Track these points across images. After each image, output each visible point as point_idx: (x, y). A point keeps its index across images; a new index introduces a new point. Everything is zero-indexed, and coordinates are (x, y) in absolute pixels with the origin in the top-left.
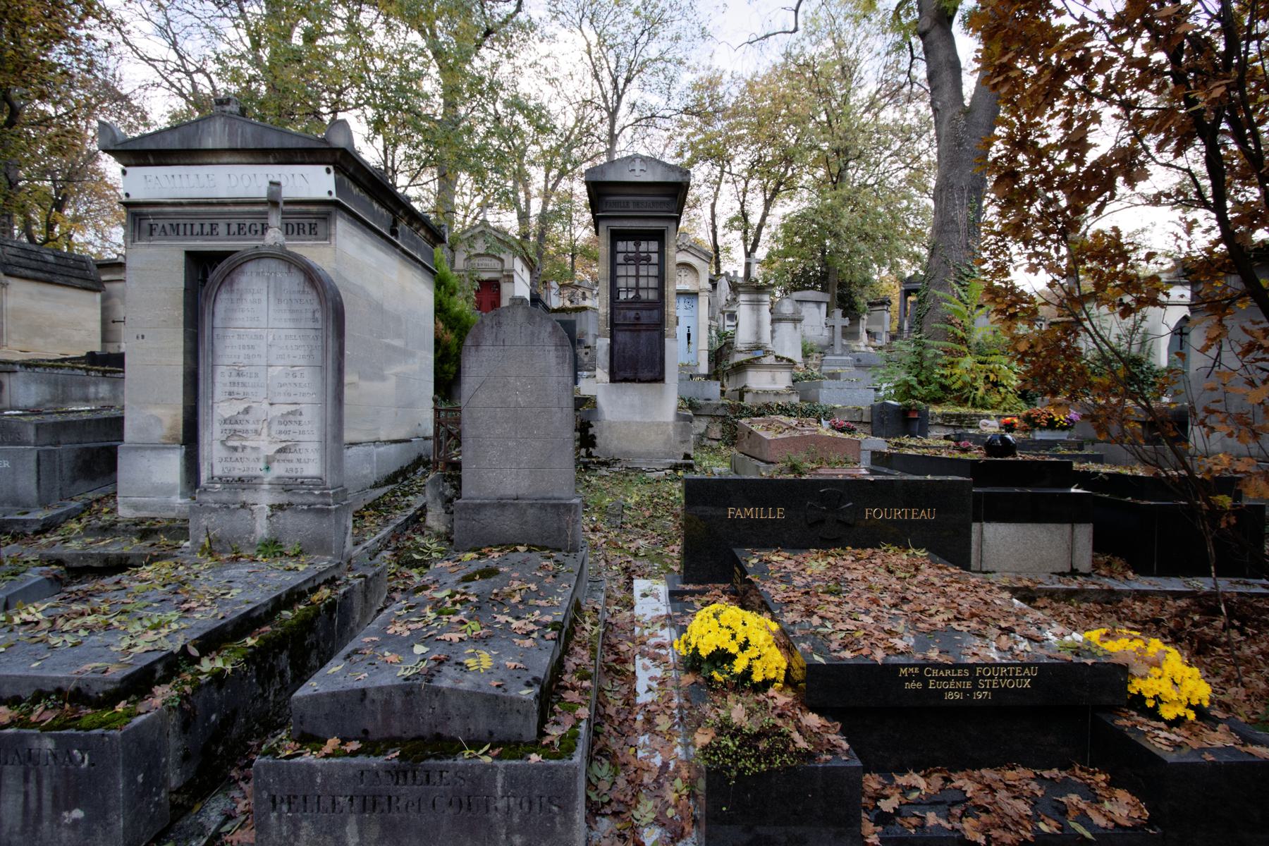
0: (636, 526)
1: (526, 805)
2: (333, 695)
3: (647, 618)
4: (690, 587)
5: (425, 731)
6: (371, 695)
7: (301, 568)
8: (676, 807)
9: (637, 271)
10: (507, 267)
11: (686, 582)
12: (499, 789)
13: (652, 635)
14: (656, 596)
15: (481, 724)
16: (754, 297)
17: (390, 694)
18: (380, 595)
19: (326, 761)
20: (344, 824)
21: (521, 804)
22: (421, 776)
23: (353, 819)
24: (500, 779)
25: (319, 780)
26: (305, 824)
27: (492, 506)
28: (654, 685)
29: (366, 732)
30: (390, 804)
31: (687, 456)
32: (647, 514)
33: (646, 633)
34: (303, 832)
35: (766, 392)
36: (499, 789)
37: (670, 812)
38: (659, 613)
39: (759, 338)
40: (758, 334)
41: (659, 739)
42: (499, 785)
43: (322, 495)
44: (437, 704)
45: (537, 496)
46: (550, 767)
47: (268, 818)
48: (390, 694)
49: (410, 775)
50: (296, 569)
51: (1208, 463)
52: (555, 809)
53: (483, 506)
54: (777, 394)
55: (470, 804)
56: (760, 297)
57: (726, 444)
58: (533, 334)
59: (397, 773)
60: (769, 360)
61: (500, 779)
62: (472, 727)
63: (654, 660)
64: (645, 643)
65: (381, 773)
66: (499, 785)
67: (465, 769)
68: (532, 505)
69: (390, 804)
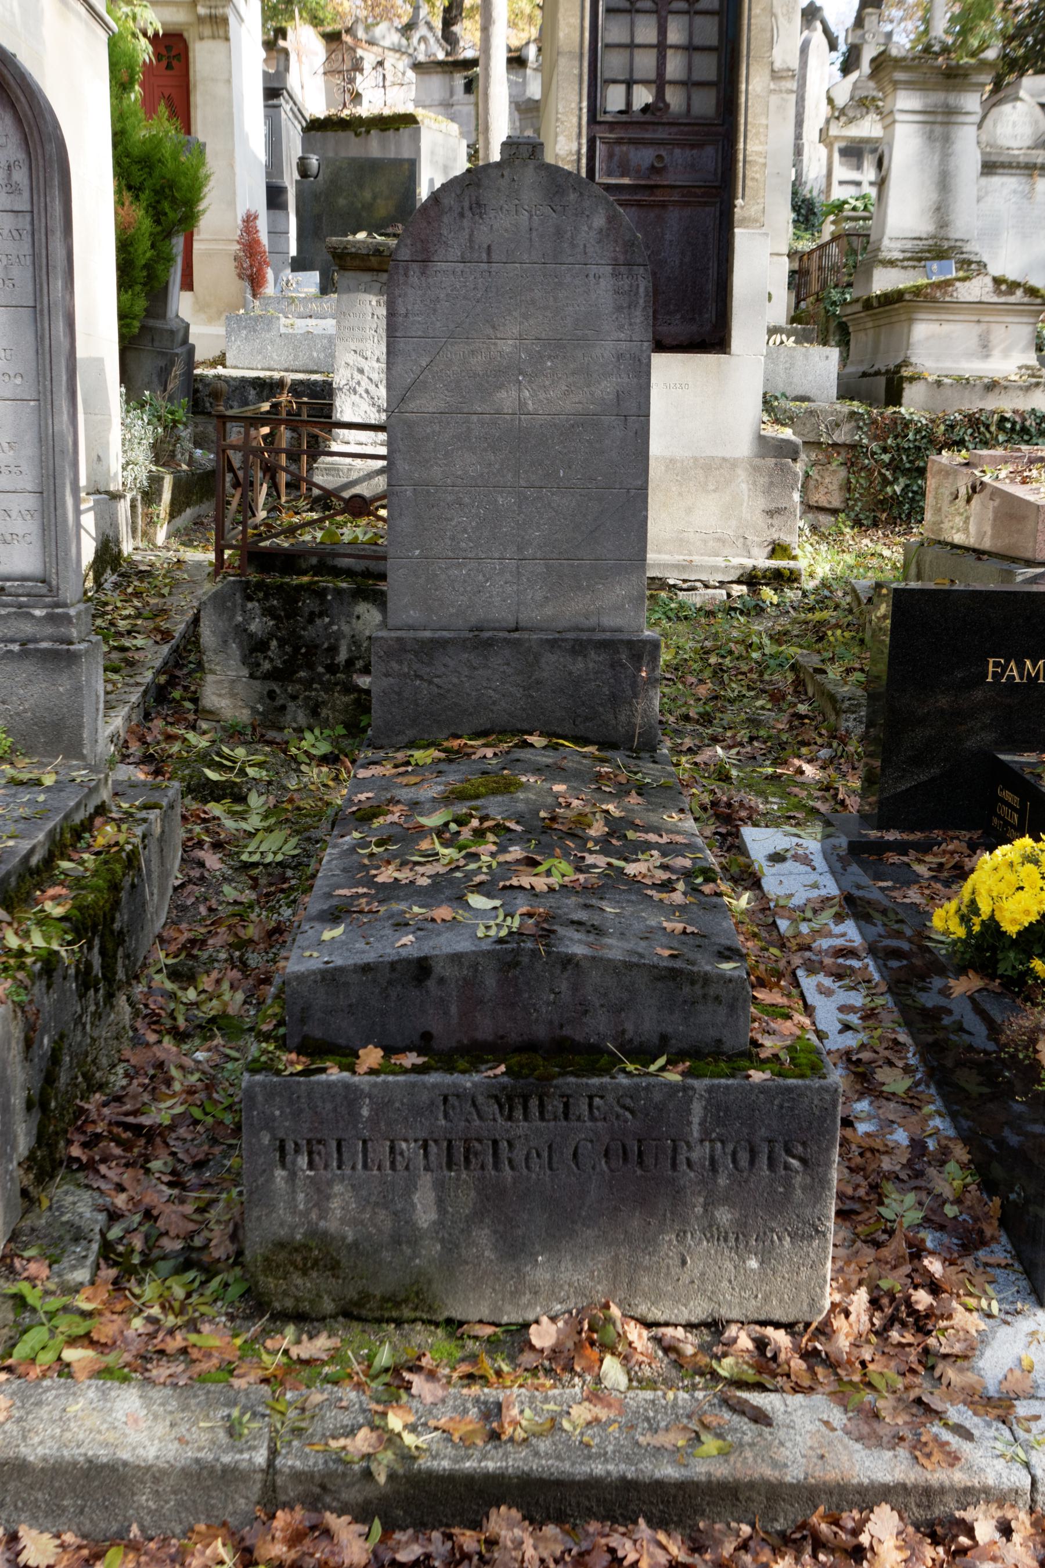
0: (686, 718)
1: (744, 1157)
2: (366, 969)
3: (798, 900)
4: (891, 836)
5: (541, 1032)
6: (438, 969)
7: (49, 780)
8: (958, 1201)
9: (662, 31)
11: (883, 825)
12: (696, 1128)
13: (817, 933)
14: (805, 860)
15: (646, 1021)
16: (937, 98)
17: (475, 967)
18: (175, 851)
19: (373, 1078)
20: (411, 1187)
21: (734, 1154)
22: (555, 1105)
23: (426, 1180)
24: (697, 1109)
25: (365, 1112)
26: (338, 1188)
27: (462, 644)
28: (854, 1019)
29: (427, 1036)
30: (496, 1154)
31: (778, 550)
32: (703, 691)
33: (804, 928)
34: (335, 1204)
35: (964, 383)
36: (696, 1128)
37: (951, 1211)
38: (823, 892)
40: (941, 212)
41: (892, 1105)
42: (696, 1120)
43: (51, 618)
44: (564, 986)
46: (789, 1089)
47: (271, 1179)
48: (475, 967)
49: (534, 1103)
50: (38, 783)
51: (874, 18)
52: (795, 1163)
53: (441, 644)
54: (992, 386)
55: (640, 1153)
56: (952, 99)
57: (857, 523)
58: (559, 233)
59: (510, 1098)
60: (977, 289)
61: (697, 1109)
62: (630, 1027)
63: (839, 977)
64: (809, 948)
65: (480, 1100)
66: (696, 1120)
67: (633, 1093)
68: (553, 644)
69: (496, 1154)
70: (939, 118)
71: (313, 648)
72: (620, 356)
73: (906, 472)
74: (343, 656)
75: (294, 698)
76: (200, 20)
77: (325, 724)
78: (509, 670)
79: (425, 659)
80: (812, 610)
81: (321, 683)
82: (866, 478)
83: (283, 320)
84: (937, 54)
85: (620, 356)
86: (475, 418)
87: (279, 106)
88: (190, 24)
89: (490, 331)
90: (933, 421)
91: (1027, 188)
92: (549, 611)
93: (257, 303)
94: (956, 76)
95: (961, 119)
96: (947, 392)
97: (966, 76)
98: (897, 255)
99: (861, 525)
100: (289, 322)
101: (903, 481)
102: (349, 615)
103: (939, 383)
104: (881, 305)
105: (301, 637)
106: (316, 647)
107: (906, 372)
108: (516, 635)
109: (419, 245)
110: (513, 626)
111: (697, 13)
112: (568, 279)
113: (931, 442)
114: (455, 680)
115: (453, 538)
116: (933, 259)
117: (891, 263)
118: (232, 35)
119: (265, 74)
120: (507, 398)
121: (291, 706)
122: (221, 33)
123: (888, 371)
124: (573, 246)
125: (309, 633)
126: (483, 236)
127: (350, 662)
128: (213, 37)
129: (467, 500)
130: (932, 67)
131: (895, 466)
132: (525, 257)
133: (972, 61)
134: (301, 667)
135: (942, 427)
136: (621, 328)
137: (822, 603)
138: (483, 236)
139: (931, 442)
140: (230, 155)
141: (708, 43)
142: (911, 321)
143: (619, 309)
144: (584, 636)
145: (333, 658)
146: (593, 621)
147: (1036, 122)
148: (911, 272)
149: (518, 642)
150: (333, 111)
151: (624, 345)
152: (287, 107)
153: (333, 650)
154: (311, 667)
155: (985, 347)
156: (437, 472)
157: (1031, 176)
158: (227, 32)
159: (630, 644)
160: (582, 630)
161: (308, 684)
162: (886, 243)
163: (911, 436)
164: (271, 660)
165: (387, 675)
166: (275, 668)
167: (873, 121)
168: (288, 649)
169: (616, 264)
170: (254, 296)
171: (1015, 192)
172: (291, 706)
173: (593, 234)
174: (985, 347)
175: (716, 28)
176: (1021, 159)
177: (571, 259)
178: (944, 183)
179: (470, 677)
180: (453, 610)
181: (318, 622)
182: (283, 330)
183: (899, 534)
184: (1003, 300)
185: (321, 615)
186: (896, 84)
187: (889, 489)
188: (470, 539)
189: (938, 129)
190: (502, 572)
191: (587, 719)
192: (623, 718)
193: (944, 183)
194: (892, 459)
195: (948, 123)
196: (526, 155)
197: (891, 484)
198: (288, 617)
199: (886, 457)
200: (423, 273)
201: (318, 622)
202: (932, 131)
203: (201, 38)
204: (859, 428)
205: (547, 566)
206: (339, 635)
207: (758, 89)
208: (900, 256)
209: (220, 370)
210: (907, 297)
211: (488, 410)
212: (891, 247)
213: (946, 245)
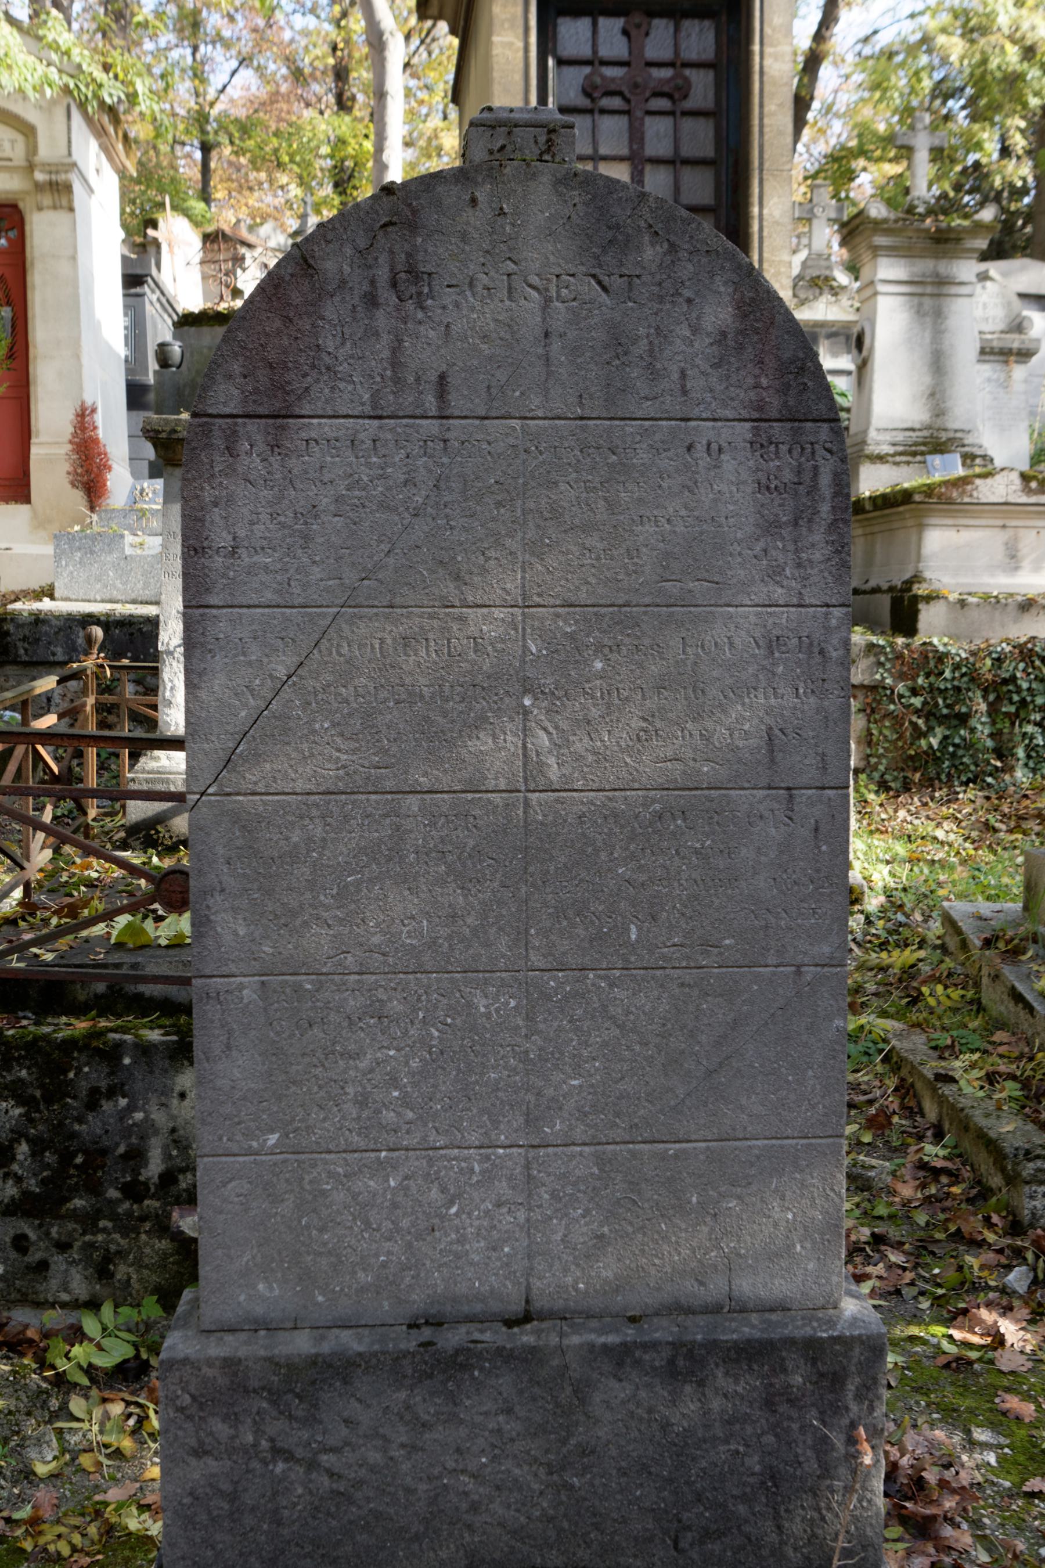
9: (636, 135)
10: (45, 152)
16: (925, 266)
27: (389, 1366)
35: (993, 602)
39: (939, 411)
40: (937, 397)
45: (638, 1299)
53: (334, 1371)
56: (944, 267)
57: (883, 786)
58: (618, 343)
68: (621, 1357)
70: (929, 290)
71: (97, 1154)
72: (773, 644)
73: (942, 720)
74: (154, 1168)
75: (63, 1247)
76: (38, 187)
77: (123, 1297)
78: (511, 1427)
79: (299, 1410)
80: (883, 946)
81: (114, 1217)
82: (892, 727)
83: (129, 538)
84: (923, 217)
85: (773, 644)
86: (413, 802)
87: (142, 295)
88: (27, 193)
89: (450, 589)
90: (973, 654)
91: (1003, 376)
92: (606, 1269)
93: (95, 517)
94: (947, 241)
95: (954, 290)
96: (974, 614)
97: (958, 240)
98: (886, 449)
99: (888, 789)
100: (138, 540)
101: (940, 731)
102: (166, 1092)
103: (962, 603)
104: (876, 508)
105: (74, 1135)
106: (104, 1152)
107: (920, 590)
108: (526, 1337)
109: (262, 374)
110: (517, 1307)
111: (685, 113)
112: (643, 456)
113: (973, 680)
114: (375, 1457)
115: (362, 1101)
116: (930, 453)
117: (881, 459)
118: (77, 204)
119: (125, 259)
120: (494, 751)
121: (58, 1262)
122: (64, 202)
123: (891, 589)
124: (654, 374)
125: (89, 1128)
126: (426, 352)
127: (168, 1178)
128: (55, 208)
129: (396, 1006)
130: (919, 230)
131: (929, 713)
132: (535, 401)
133: (966, 223)
134: (74, 1191)
135: (988, 662)
136: (775, 573)
137: (898, 937)
138: (426, 352)
139: (973, 680)
140: (75, 345)
141: (699, 153)
142: (921, 527)
143: (770, 527)
144: (697, 1330)
145: (136, 1172)
146: (716, 1289)
147: (1009, 304)
148: (905, 470)
149: (531, 1356)
150: (209, 305)
151: (785, 617)
152: (151, 296)
153: (136, 1156)
154: (94, 1189)
155: (1013, 557)
156: (319, 940)
157: (1006, 362)
158: (71, 201)
159: (812, 1349)
160: (689, 1311)
161: (89, 1221)
162: (872, 434)
163: (947, 674)
164: (19, 1179)
165: (200, 1452)
166: (26, 1194)
167: (828, 303)
168: (49, 1157)
169: (760, 418)
170: (92, 509)
171: (989, 380)
172: (58, 1262)
173: (702, 343)
174: (1013, 557)
175: (711, 134)
176: (995, 344)
177: (649, 408)
178: (938, 363)
179: (412, 1448)
180: (365, 1278)
181: (107, 1106)
182: (128, 551)
183: (942, 802)
184: (1033, 499)
185: (112, 1093)
186: (876, 251)
187: (923, 742)
188: (405, 1101)
189: (927, 302)
190: (488, 1178)
191: (706, 1535)
192: (796, 1527)
193: (938, 363)
194: (925, 703)
195: (939, 295)
196: (531, 152)
197: (925, 735)
198: (49, 1099)
199: (917, 701)
200: (274, 446)
201: (107, 1106)
202: (920, 305)
203: (40, 209)
204: (881, 664)
205: (600, 1160)
206: (147, 1129)
207: (777, 213)
208: (891, 450)
209: (46, 605)
210: (917, 498)
211: (446, 781)
212: (878, 441)
213: (944, 436)
